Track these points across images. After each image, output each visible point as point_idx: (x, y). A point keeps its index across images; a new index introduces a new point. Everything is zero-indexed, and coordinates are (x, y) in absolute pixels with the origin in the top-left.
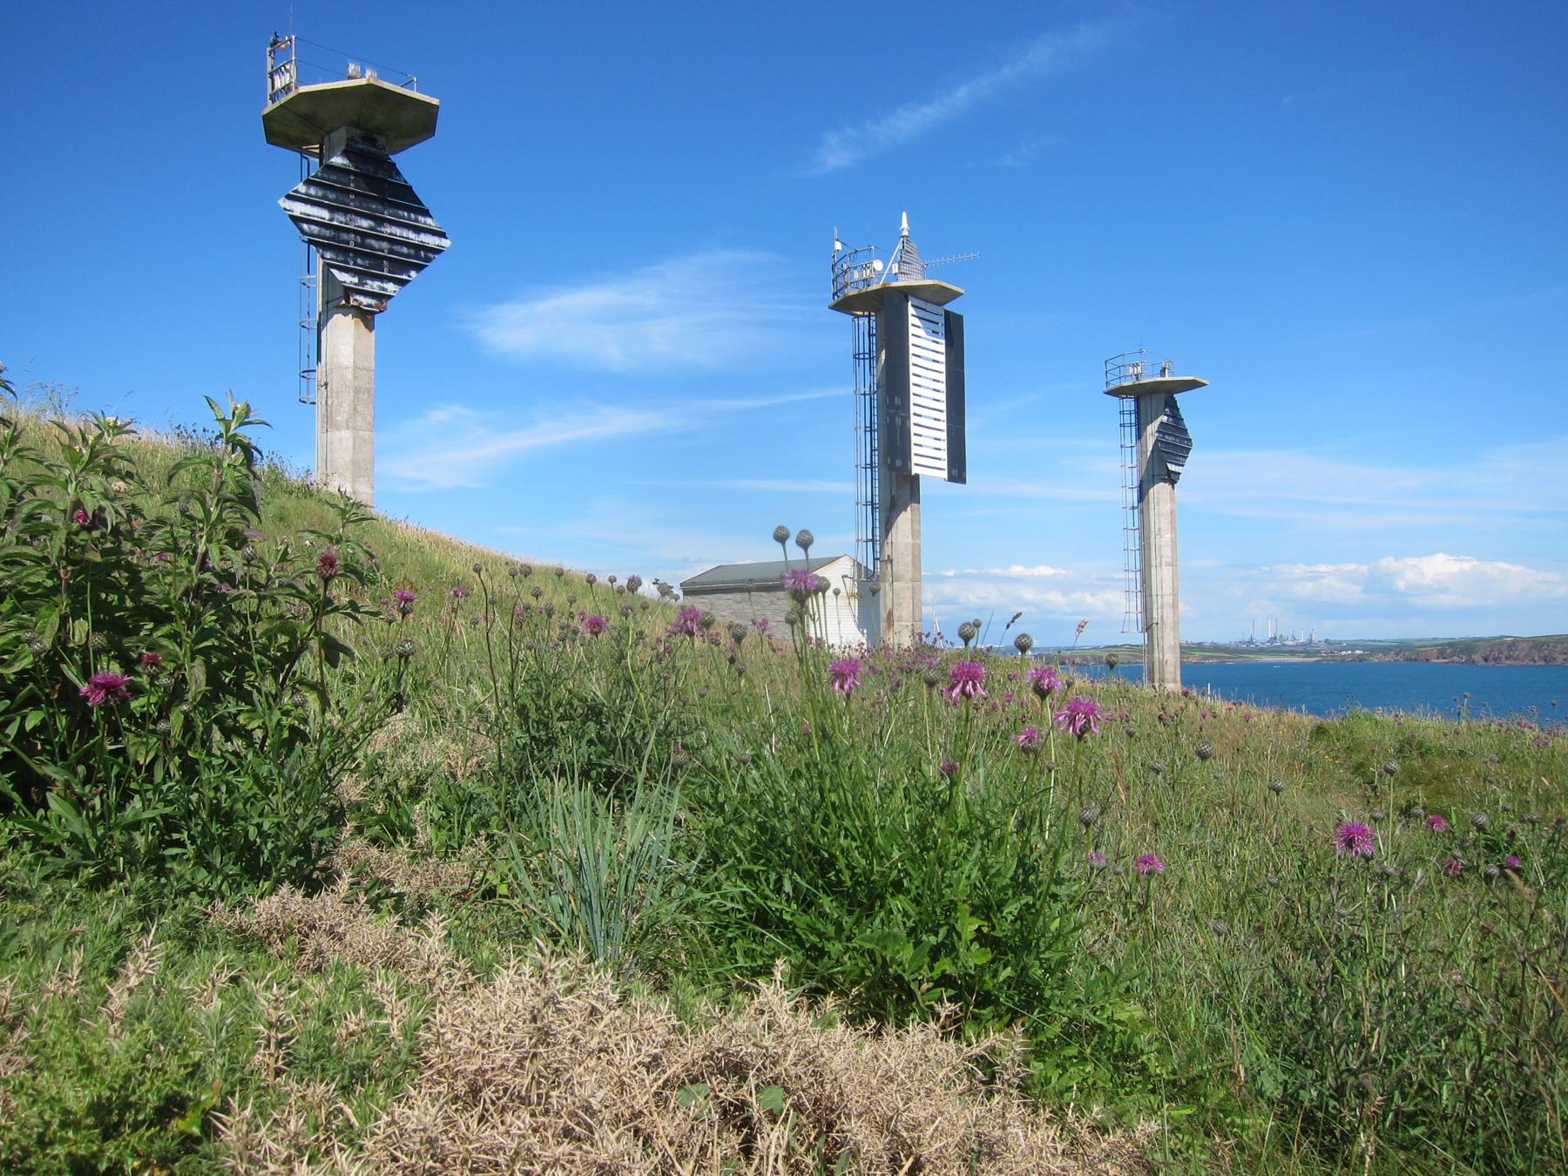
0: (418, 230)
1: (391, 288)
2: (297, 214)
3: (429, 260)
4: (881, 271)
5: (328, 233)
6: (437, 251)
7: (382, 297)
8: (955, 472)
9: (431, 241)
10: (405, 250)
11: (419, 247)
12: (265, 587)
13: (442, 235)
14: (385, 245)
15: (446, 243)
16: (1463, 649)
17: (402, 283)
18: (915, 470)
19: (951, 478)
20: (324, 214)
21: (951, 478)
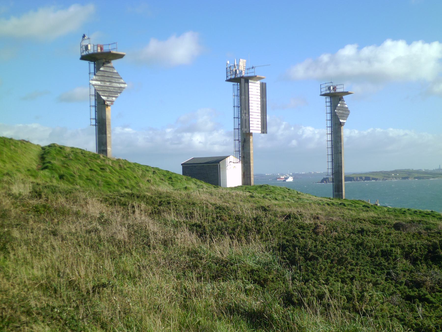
0: (119, 83)
1: (114, 98)
2: (94, 84)
3: (122, 90)
4: (242, 67)
5: (100, 87)
6: (124, 88)
7: (112, 102)
8: (264, 86)
9: (122, 85)
10: (117, 89)
11: (121, 87)
12: (76, 233)
13: (125, 83)
14: (112, 88)
15: (126, 85)
16: (385, 172)
17: (116, 97)
18: (251, 131)
19: (263, 132)
20: (99, 83)
21: (263, 132)
